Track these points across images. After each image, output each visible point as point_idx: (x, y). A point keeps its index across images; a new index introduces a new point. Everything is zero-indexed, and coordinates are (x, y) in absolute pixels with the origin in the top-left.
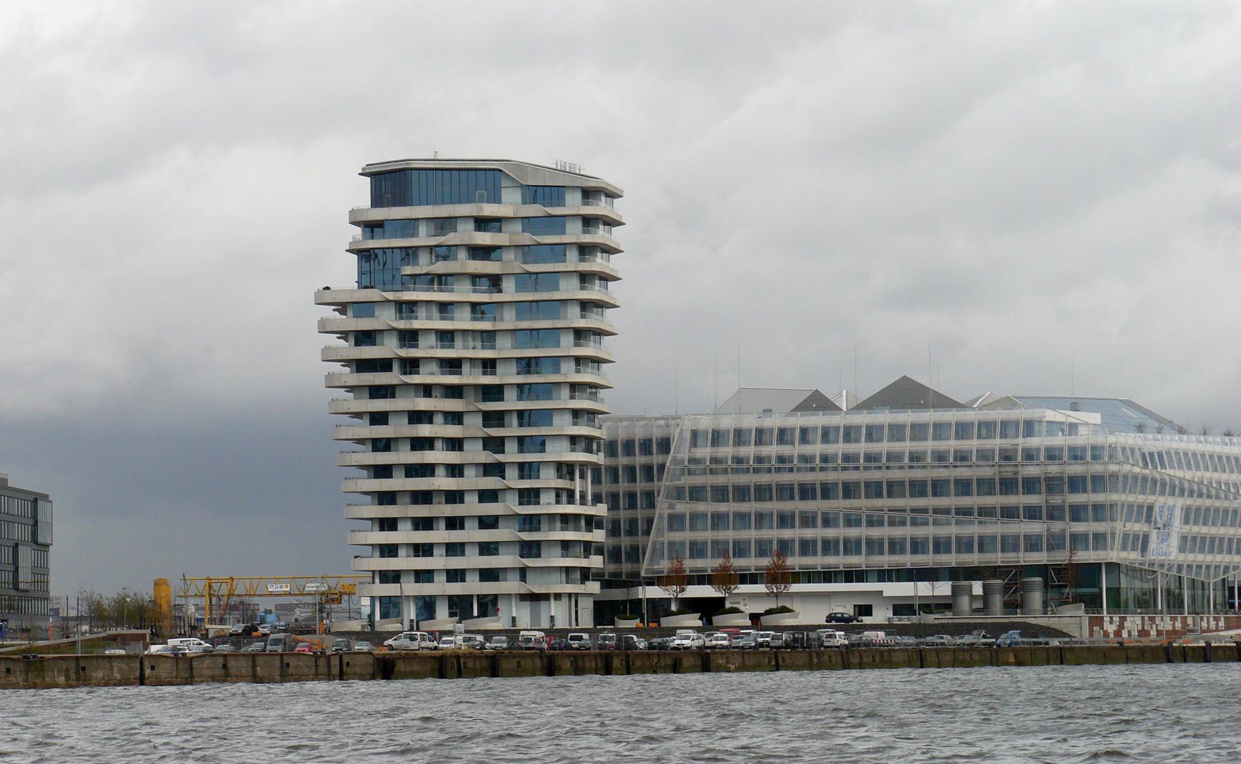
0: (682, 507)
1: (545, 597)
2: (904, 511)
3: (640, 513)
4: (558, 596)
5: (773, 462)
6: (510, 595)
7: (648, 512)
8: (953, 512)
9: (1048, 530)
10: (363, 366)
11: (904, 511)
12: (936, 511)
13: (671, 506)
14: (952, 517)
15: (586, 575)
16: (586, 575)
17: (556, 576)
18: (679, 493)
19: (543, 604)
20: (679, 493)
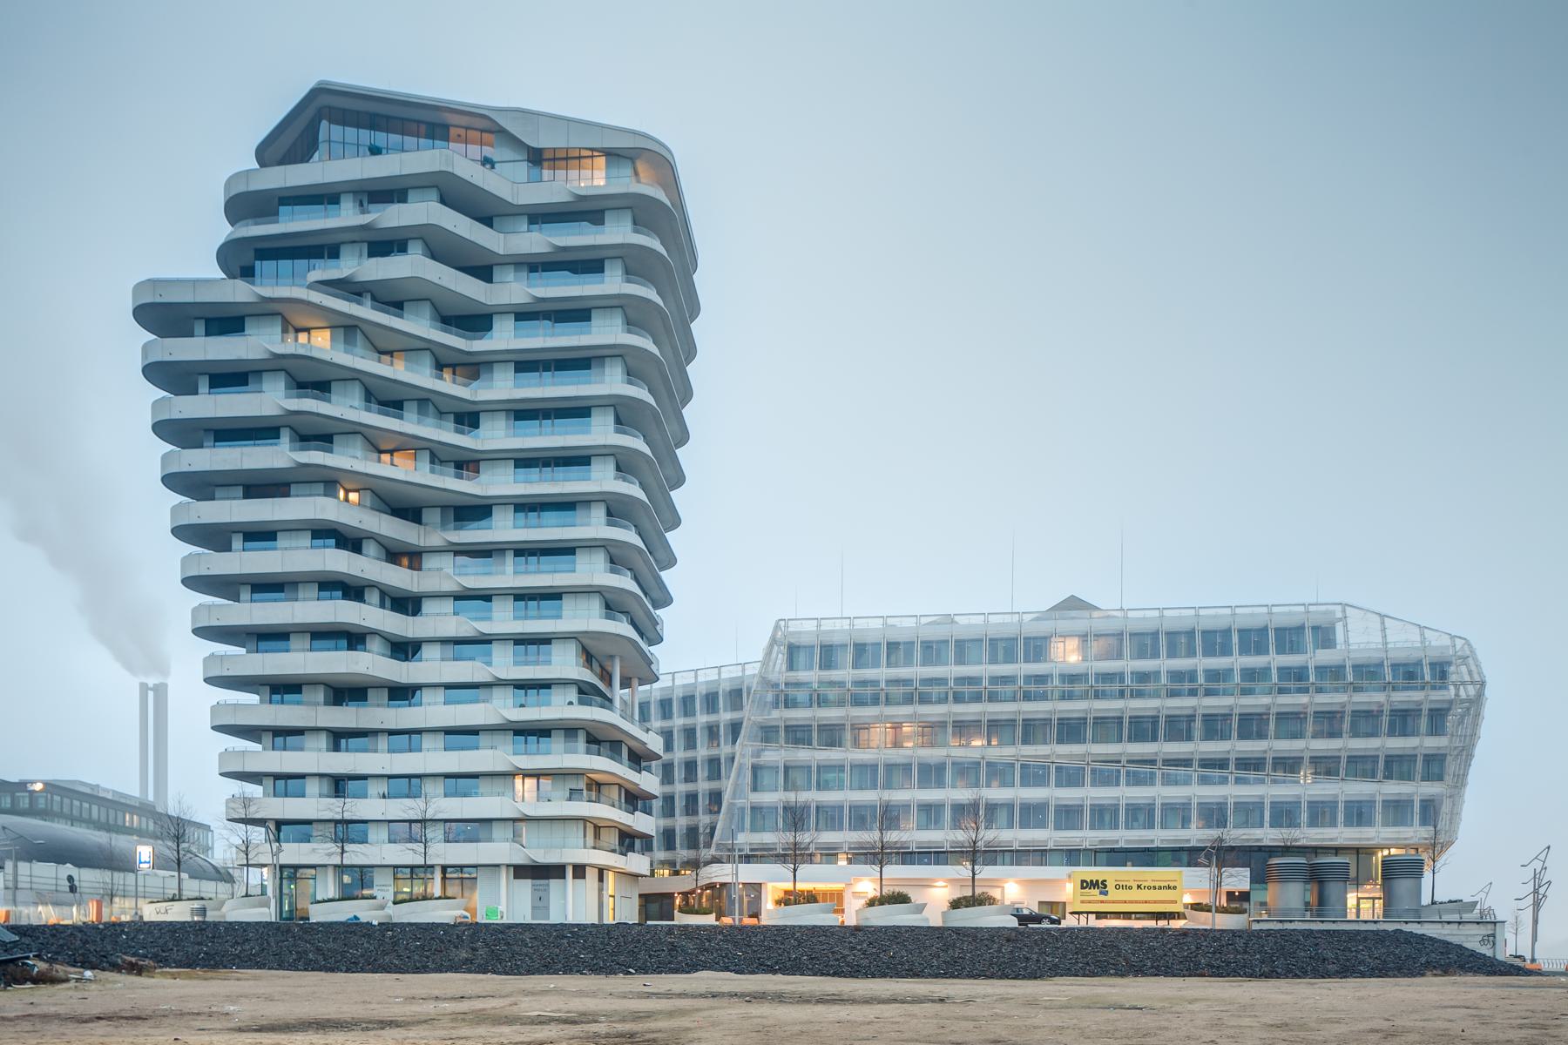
0: (775, 756)
1: (557, 871)
2: (1153, 762)
3: (703, 786)
4: (580, 871)
5: (1128, 681)
6: (498, 866)
7: (714, 785)
8: (1195, 764)
9: (489, 664)
10: (214, 537)
11: (1153, 762)
12: (1168, 762)
13: (757, 754)
14: (1195, 772)
15: (628, 840)
16: (628, 840)
17: (575, 834)
18: (768, 733)
19: (554, 884)
20: (768, 733)
